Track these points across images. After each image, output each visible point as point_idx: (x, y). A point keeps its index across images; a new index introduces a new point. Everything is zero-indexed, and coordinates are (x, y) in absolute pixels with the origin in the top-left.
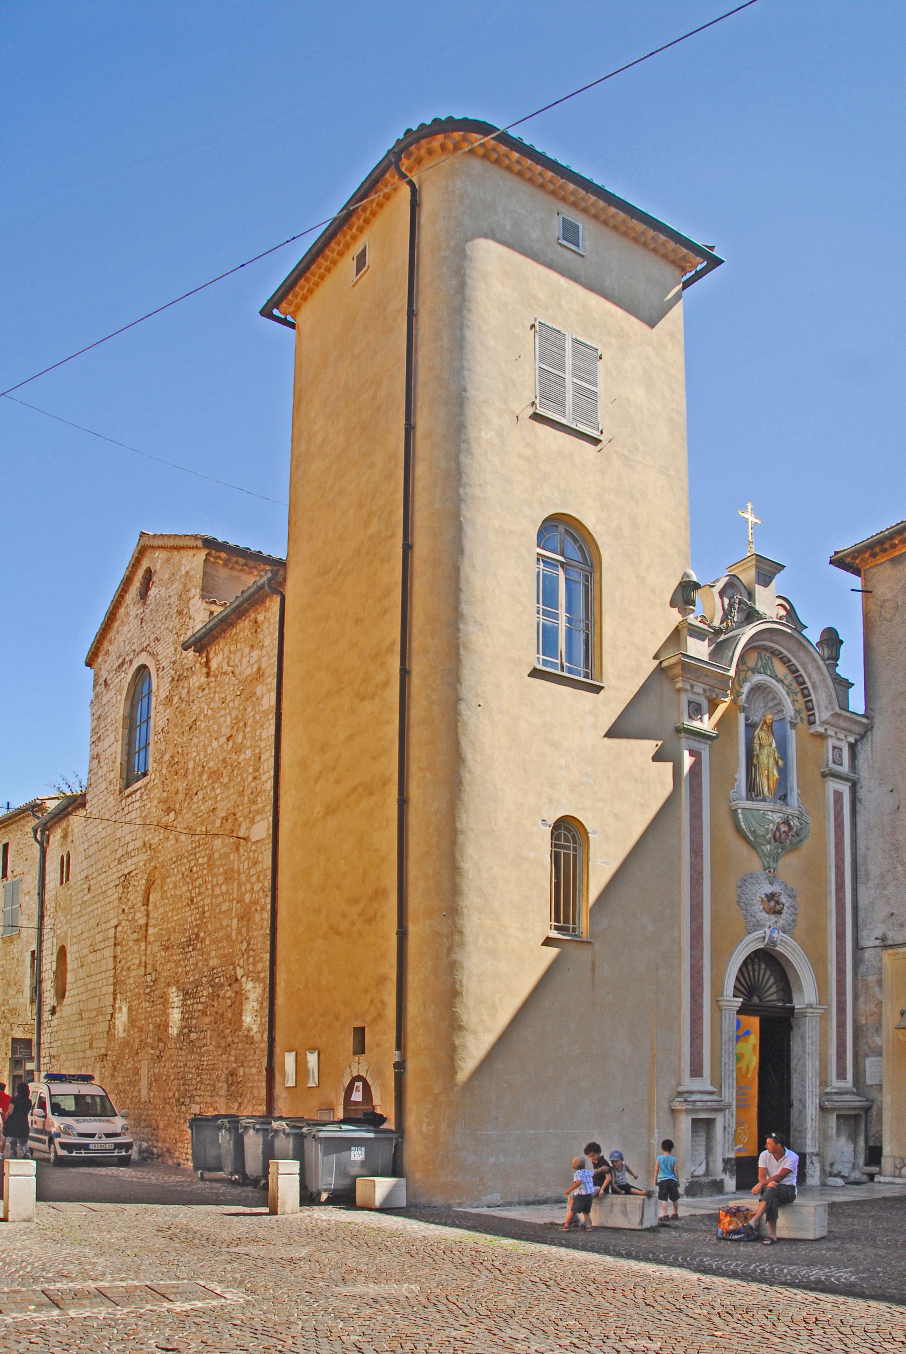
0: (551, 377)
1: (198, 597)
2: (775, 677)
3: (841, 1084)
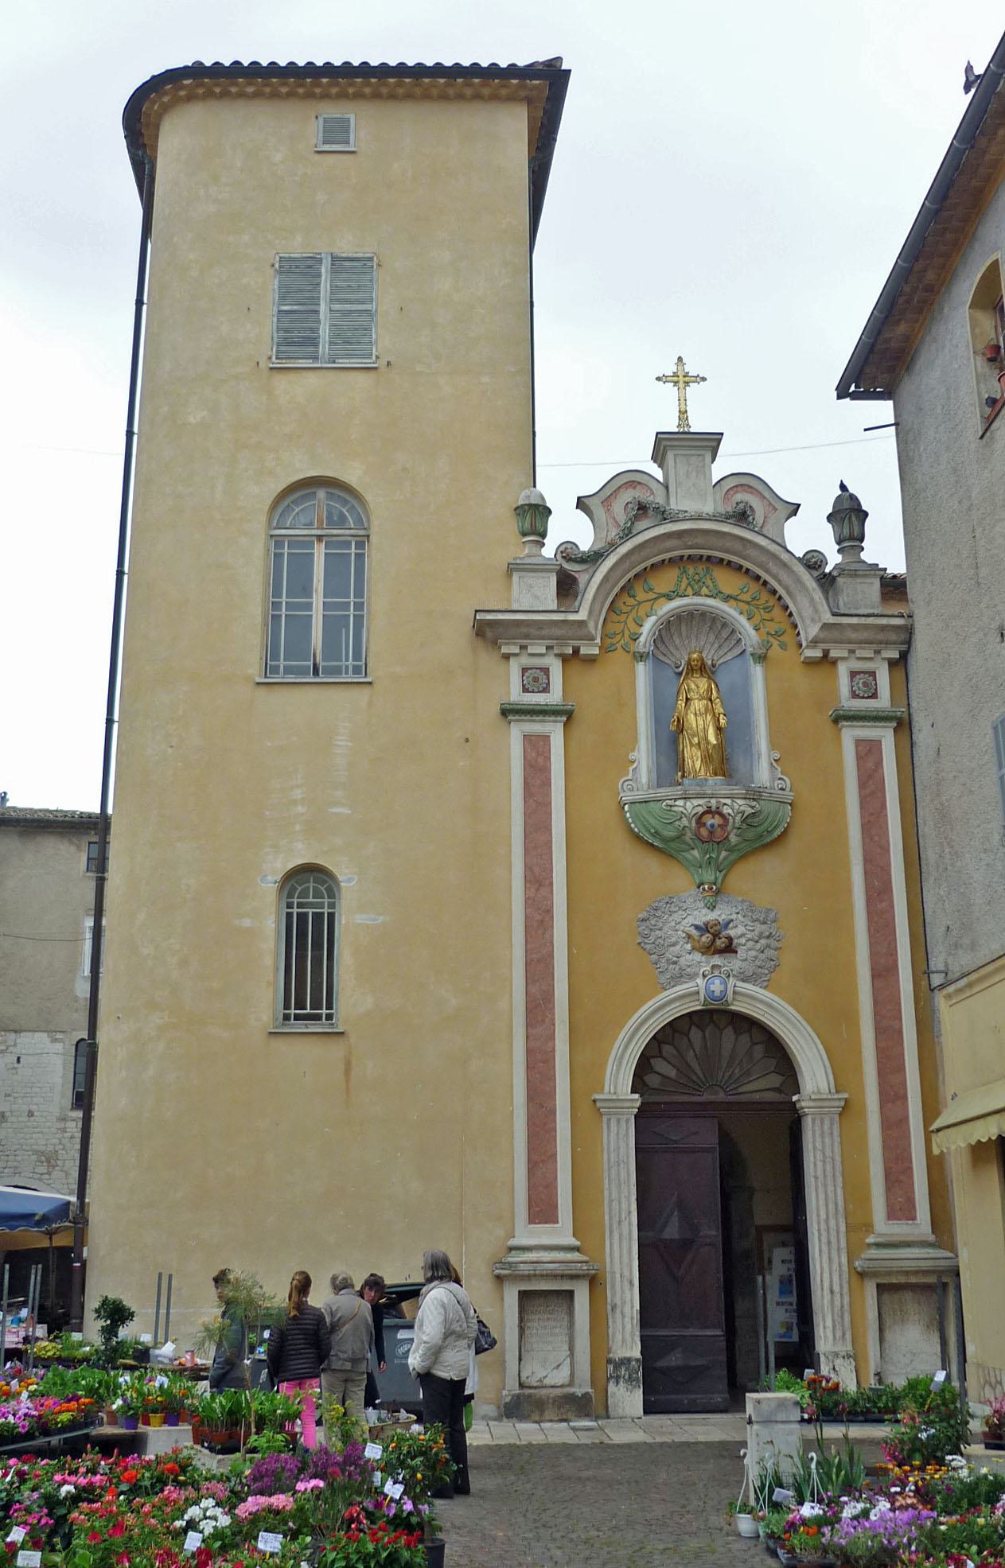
3: (900, 1230)
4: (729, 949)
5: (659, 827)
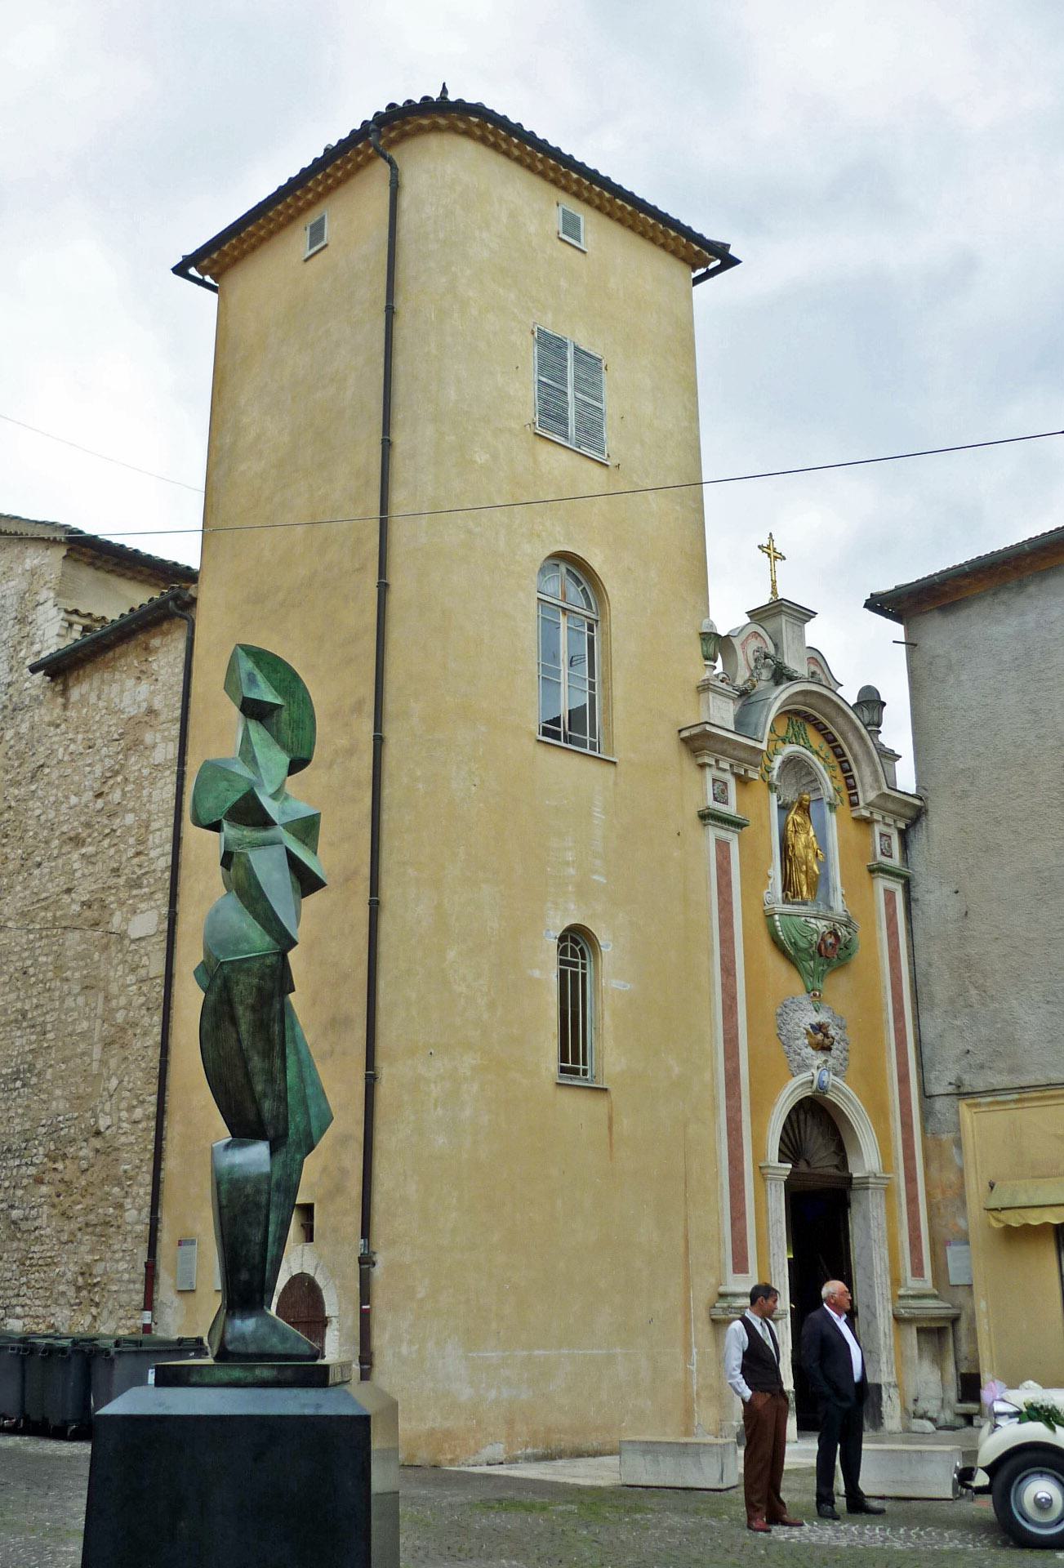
0: (550, 391)
1: (50, 603)
2: (809, 748)
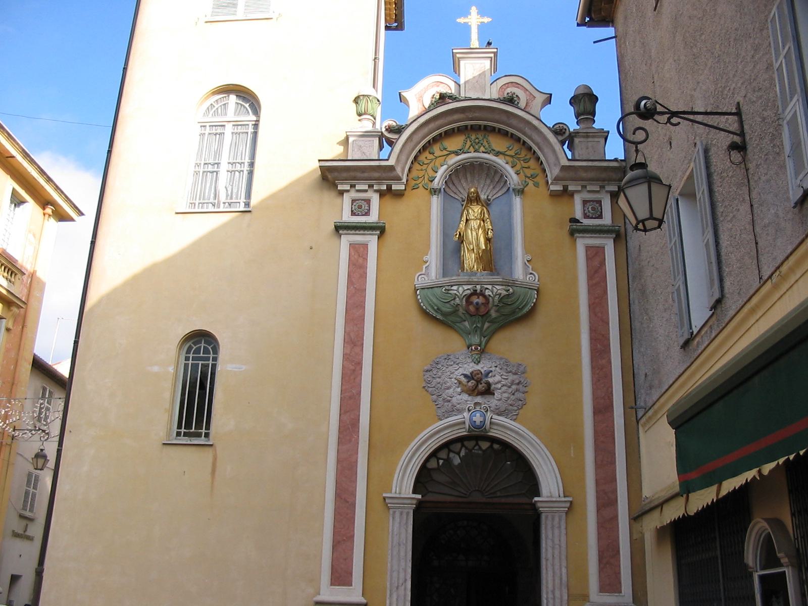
4: (488, 391)
5: (440, 305)
